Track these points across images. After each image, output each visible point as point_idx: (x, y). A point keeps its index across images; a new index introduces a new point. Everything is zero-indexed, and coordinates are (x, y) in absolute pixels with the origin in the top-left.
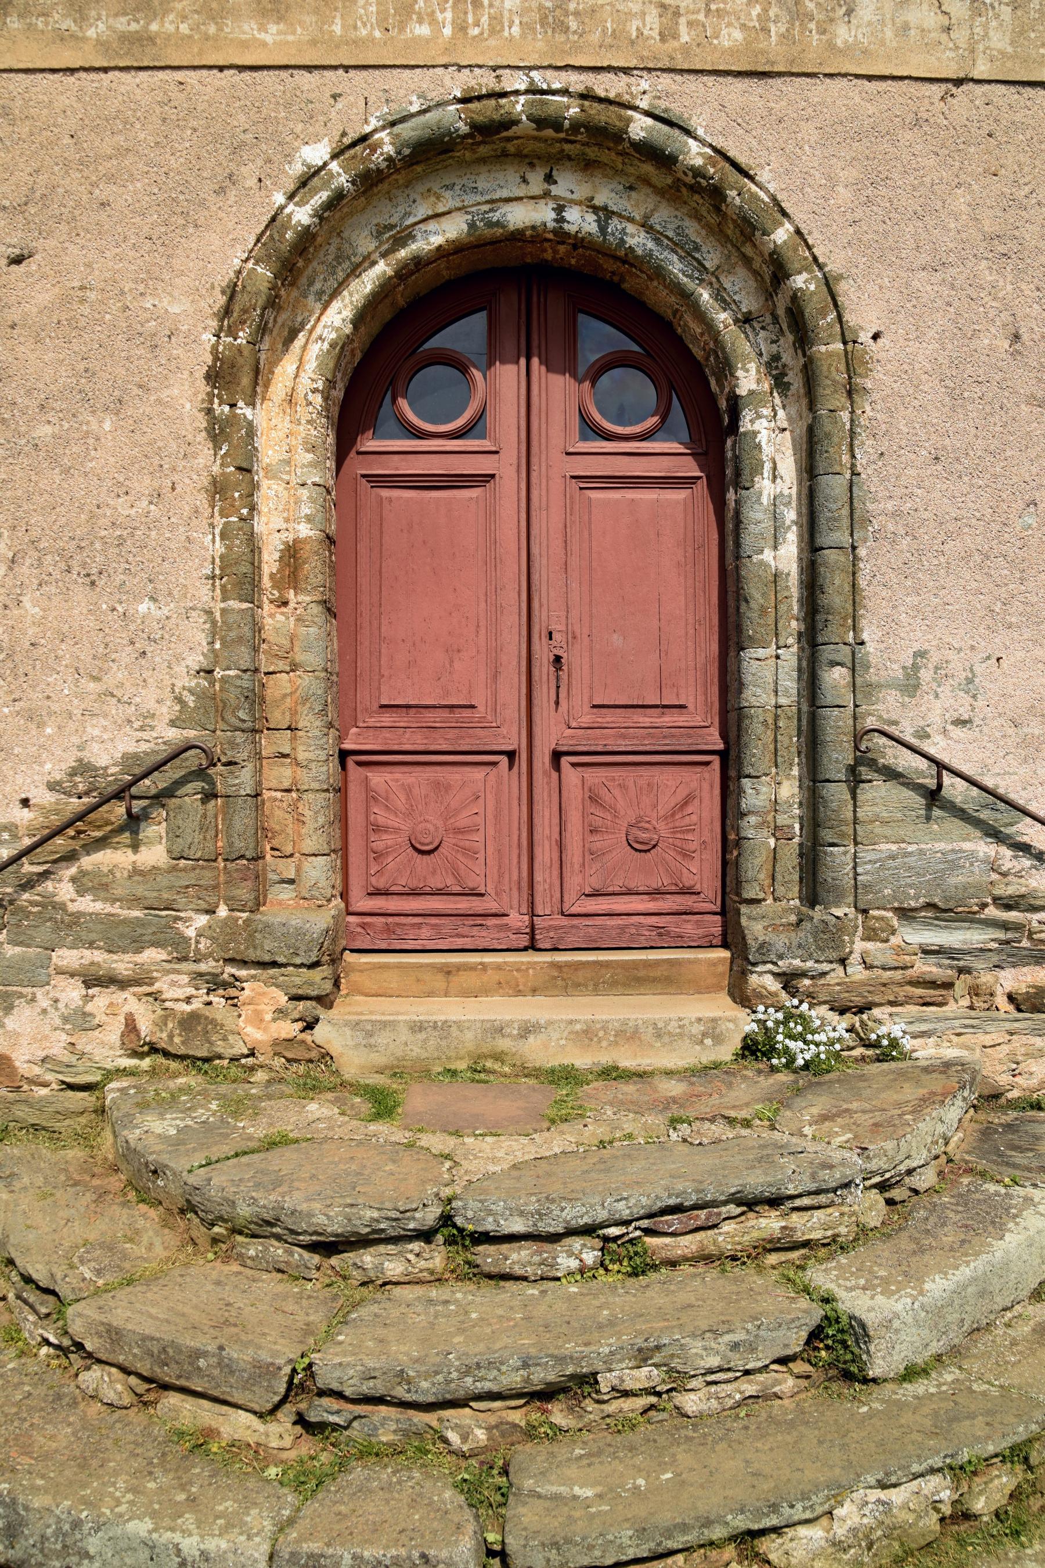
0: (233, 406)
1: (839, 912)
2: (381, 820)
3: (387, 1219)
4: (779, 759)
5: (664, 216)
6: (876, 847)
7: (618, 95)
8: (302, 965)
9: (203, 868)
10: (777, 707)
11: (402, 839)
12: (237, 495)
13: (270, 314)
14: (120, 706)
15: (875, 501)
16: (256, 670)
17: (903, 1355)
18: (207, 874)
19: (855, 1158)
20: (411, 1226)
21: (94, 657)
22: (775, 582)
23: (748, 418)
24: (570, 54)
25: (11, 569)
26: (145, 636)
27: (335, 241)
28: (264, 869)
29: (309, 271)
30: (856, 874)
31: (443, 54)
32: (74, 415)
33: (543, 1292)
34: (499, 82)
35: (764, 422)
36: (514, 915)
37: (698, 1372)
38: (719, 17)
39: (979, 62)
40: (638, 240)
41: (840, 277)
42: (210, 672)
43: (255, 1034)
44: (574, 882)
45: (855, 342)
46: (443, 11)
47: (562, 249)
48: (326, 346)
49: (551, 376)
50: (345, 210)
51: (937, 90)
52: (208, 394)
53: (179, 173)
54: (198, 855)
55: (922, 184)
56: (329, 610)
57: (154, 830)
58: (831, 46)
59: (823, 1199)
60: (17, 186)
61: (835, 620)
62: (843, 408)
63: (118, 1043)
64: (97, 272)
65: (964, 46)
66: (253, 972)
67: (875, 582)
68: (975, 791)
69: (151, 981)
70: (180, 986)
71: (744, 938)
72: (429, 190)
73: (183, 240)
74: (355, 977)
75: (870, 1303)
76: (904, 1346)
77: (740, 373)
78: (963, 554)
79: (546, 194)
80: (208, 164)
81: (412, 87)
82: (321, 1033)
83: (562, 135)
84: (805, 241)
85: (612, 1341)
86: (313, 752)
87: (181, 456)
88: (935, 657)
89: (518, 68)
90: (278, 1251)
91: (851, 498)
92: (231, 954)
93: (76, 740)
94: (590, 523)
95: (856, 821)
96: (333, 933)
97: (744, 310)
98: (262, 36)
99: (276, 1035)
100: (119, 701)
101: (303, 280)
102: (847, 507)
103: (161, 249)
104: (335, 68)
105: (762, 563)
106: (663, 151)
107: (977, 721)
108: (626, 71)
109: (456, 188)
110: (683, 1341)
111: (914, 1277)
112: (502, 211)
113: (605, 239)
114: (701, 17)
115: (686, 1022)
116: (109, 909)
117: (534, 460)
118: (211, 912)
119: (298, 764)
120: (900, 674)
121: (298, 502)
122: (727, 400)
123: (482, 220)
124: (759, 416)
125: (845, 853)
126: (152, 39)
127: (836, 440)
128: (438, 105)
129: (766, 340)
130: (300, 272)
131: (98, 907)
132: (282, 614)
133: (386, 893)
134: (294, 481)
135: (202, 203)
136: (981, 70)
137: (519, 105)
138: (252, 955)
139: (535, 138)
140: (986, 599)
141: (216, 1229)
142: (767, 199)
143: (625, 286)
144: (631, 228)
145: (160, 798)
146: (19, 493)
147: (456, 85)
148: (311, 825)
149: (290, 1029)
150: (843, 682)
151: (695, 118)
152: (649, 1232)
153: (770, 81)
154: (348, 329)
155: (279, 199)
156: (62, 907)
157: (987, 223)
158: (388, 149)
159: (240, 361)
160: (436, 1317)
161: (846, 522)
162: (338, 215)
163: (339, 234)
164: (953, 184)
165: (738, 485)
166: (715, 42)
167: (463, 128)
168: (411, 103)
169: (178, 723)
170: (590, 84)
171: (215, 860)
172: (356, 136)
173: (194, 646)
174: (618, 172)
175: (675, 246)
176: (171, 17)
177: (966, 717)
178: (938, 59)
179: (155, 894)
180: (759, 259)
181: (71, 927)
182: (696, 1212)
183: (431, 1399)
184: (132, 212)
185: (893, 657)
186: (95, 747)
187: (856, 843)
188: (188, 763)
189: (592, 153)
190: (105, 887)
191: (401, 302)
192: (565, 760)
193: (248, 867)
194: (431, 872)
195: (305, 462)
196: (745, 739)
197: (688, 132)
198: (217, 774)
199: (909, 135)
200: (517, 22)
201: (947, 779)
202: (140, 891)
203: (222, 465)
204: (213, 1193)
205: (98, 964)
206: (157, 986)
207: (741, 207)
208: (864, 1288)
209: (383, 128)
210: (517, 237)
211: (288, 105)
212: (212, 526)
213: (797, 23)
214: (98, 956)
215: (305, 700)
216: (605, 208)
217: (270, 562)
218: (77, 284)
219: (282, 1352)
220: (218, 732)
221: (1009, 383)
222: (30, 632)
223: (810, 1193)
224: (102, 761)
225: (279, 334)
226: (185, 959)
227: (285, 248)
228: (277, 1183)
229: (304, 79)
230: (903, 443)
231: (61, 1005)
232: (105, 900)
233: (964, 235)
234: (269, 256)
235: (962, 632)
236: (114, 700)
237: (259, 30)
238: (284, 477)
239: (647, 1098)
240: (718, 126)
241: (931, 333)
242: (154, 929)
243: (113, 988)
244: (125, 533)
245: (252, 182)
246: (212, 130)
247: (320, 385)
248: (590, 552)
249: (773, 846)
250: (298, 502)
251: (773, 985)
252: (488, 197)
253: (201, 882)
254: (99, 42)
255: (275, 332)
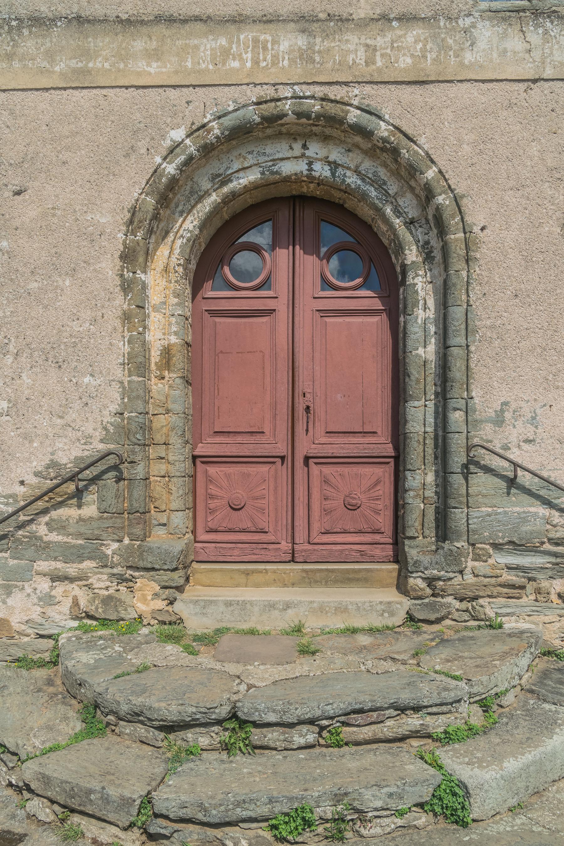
0: (134, 273)
1: (459, 545)
2: (213, 492)
3: (200, 713)
4: (426, 461)
5: (367, 165)
6: (480, 509)
7: (342, 98)
8: (168, 570)
9: (116, 518)
10: (425, 432)
11: (225, 502)
12: (136, 320)
13: (155, 224)
14: (74, 432)
15: (480, 320)
16: (147, 413)
17: (490, 806)
18: (118, 520)
19: (464, 685)
20: (213, 717)
21: (60, 406)
22: (425, 365)
23: (411, 276)
24: (315, 75)
25: (16, 359)
26: (87, 395)
27: (190, 183)
28: (150, 518)
29: (176, 200)
30: (468, 524)
31: (247, 77)
32: (49, 277)
33: (285, 757)
34: (276, 93)
35: (420, 279)
36: (283, 543)
37: (369, 810)
38: (398, 50)
39: (547, 69)
40: (352, 180)
41: (463, 196)
42: (122, 414)
43: (141, 607)
44: (316, 527)
45: (471, 232)
46: (246, 53)
47: (312, 186)
48: (185, 240)
49: (305, 256)
50: (194, 166)
51: (522, 86)
52: (121, 266)
53: (105, 146)
54: (114, 510)
55: (512, 141)
56: (187, 381)
57: (90, 497)
58: (462, 64)
59: (444, 709)
60: (18, 152)
61: (456, 385)
62: (463, 269)
63: (68, 612)
64: (61, 200)
65: (538, 60)
66: (142, 573)
67: (479, 364)
68: (537, 480)
69: (87, 578)
70: (103, 581)
71: (406, 558)
72: (240, 155)
73: (107, 183)
74: (198, 576)
75: (471, 773)
76: (491, 801)
77: (407, 252)
78: (530, 348)
79: (303, 155)
80: (120, 140)
81: (230, 96)
82: (178, 607)
83: (311, 122)
84: (444, 177)
85: (320, 789)
86: (178, 457)
87: (107, 299)
88: (513, 406)
89: (287, 84)
90: (141, 730)
91: (467, 319)
92: (130, 564)
93: (50, 449)
94: (326, 335)
95: (468, 495)
96: (185, 552)
97: (410, 217)
98: (149, 69)
99: (153, 608)
100: (73, 429)
101: (173, 205)
102: (464, 324)
103: (96, 188)
104: (188, 86)
105: (417, 355)
106: (366, 129)
107: (538, 440)
108: (346, 84)
109: (255, 153)
110: (360, 791)
111: (498, 758)
112: (279, 165)
113: (334, 180)
114: (388, 51)
115: (374, 603)
116: (66, 539)
117: (296, 301)
118: (120, 541)
119: (169, 463)
120: (493, 415)
121: (170, 324)
122: (401, 267)
123: (268, 171)
124: (417, 275)
125: (462, 512)
126: (89, 72)
127: (458, 287)
128: (244, 106)
129: (422, 233)
130: (171, 200)
131: (60, 538)
132: (161, 383)
133: (216, 531)
134: (168, 313)
135: (117, 162)
136: (549, 73)
137: (287, 106)
138: (141, 564)
139: (297, 124)
140: (544, 373)
141: (109, 717)
142: (423, 154)
143: (346, 206)
144: (349, 173)
145: (94, 480)
146: (20, 318)
147: (253, 94)
148: (175, 495)
149: (160, 604)
150: (461, 419)
151: (384, 109)
152: (344, 724)
153: (426, 86)
154: (197, 232)
155: (158, 160)
156: (40, 538)
157: (549, 161)
158: (217, 132)
159: (138, 248)
160: (224, 771)
161: (463, 332)
162: (190, 169)
163: (191, 180)
164: (530, 140)
165: (405, 313)
166: (396, 65)
167: (257, 119)
168: (229, 106)
169: (104, 441)
170: (326, 92)
171: (123, 514)
172: (200, 125)
173: (113, 400)
174: (342, 142)
175: (373, 182)
176: (100, 59)
177: (531, 438)
178: (523, 68)
179: (91, 531)
180: (419, 188)
181: (44, 549)
182: (371, 713)
183: (217, 820)
184: (80, 167)
185: (489, 405)
186: (60, 453)
187: (468, 507)
188: (109, 462)
189: (328, 131)
190: (64, 528)
191: (226, 217)
192: (311, 461)
193: (137, 517)
194: (242, 520)
195: (174, 303)
196: (407, 450)
197: (380, 117)
198: (125, 468)
199: (505, 113)
200: (287, 58)
201: (520, 472)
202: (82, 530)
203: (128, 304)
204: (108, 697)
205: (59, 569)
206: (90, 581)
207: (409, 159)
208: (468, 764)
209: (214, 120)
210: (287, 180)
211: (163, 108)
212: (123, 337)
213: (443, 52)
214: (59, 565)
215: (173, 429)
216: (335, 162)
217: (155, 356)
218: (50, 206)
219: (136, 790)
220: (126, 446)
221: (560, 252)
222: (26, 392)
223: (436, 705)
224: (64, 461)
225: (160, 234)
226: (106, 566)
227: (162, 187)
228: (144, 692)
229: (172, 93)
230: (497, 288)
231: (38, 592)
232: (64, 535)
233: (535, 169)
234: (153, 191)
235: (529, 391)
236: (71, 429)
237: (147, 66)
238: (164, 311)
239: (350, 646)
240: (397, 113)
241: (515, 225)
242: (90, 550)
243: (66, 582)
244: (77, 340)
245: (143, 151)
246: (122, 122)
247: (182, 262)
248: (326, 351)
249: (422, 508)
250: (170, 324)
251: (421, 584)
252: (271, 158)
253: (115, 525)
254: (61, 74)
255: (158, 233)
